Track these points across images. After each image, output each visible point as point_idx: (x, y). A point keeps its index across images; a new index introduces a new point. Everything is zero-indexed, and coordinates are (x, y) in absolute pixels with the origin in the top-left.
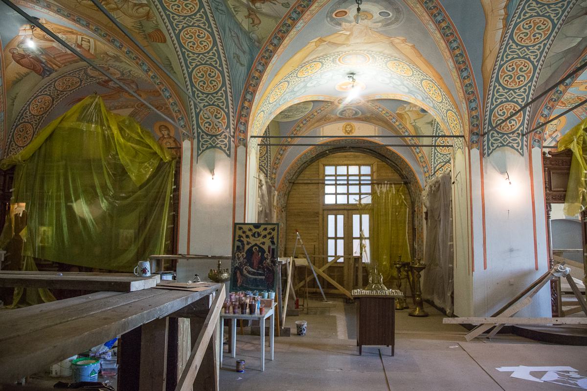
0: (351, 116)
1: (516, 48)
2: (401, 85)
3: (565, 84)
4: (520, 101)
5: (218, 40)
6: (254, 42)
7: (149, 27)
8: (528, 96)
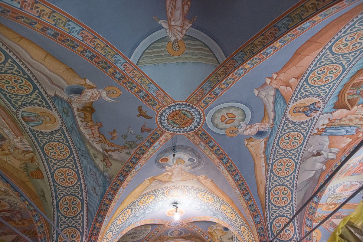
0: (178, 236)
1: (277, 179)
2: (208, 210)
3: (317, 197)
4: (288, 215)
5: (81, 177)
6: (107, 179)
7: (32, 167)
8: (293, 211)
